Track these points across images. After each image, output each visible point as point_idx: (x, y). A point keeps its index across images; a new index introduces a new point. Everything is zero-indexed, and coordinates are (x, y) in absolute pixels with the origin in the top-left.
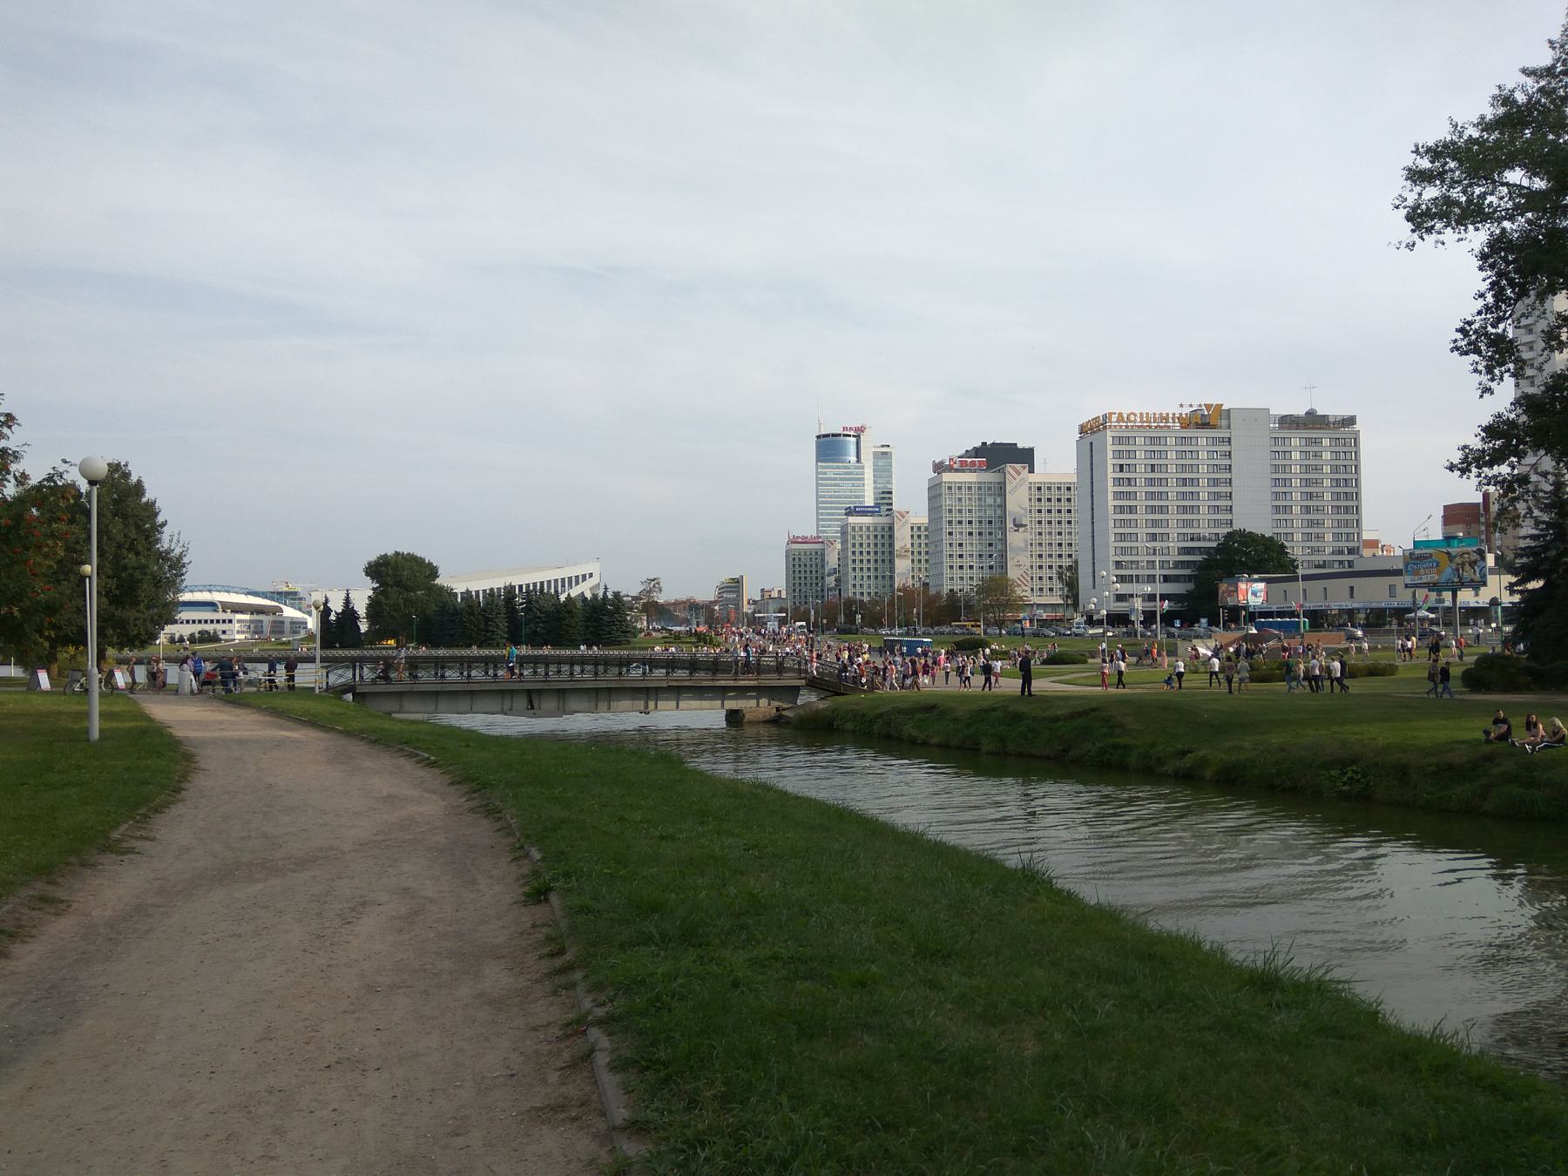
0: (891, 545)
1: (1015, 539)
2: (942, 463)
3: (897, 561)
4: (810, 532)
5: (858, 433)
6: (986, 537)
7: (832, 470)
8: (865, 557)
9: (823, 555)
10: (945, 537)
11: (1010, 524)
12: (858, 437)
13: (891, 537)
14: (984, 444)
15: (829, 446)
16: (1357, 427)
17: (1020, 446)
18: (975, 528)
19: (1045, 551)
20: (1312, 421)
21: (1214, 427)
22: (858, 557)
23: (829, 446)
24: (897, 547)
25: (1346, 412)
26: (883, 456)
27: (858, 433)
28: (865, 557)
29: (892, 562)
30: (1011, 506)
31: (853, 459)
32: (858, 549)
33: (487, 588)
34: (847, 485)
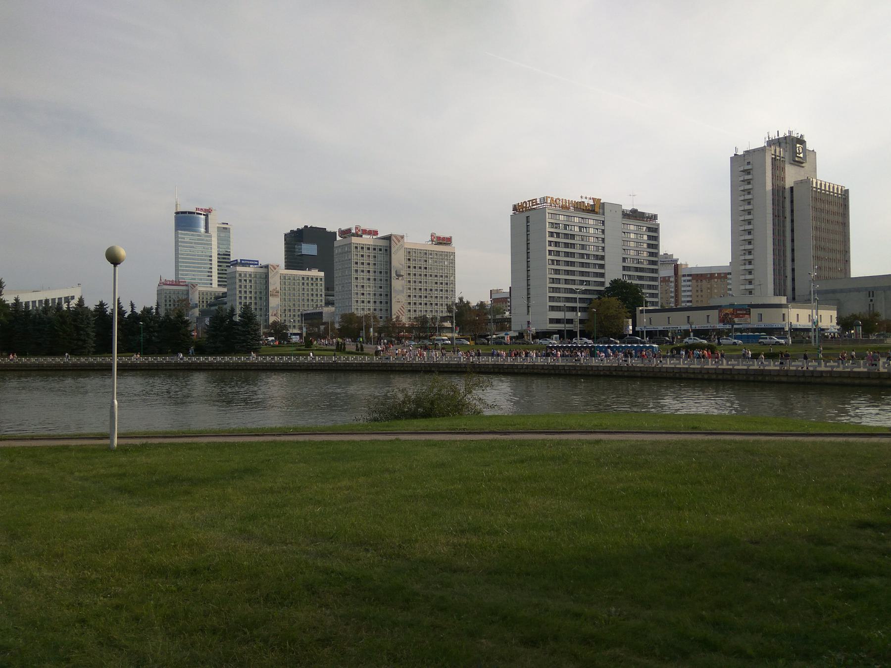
0: (267, 288)
1: (397, 284)
2: (349, 230)
3: (271, 298)
4: (171, 277)
5: (207, 213)
6: (378, 282)
7: (186, 236)
8: (248, 295)
9: (188, 294)
10: (353, 280)
11: (394, 274)
12: (207, 216)
13: (267, 282)
14: (306, 227)
15: (185, 220)
16: (658, 221)
17: (328, 230)
18: (372, 277)
19: (412, 293)
20: (634, 215)
21: (597, 213)
22: (243, 295)
23: (185, 220)
24: (271, 289)
25: (447, 236)
26: (224, 230)
27: (207, 213)
28: (248, 295)
29: (267, 300)
30: (395, 263)
31: (203, 230)
32: (243, 290)
33: (43, 298)
34: (199, 248)
